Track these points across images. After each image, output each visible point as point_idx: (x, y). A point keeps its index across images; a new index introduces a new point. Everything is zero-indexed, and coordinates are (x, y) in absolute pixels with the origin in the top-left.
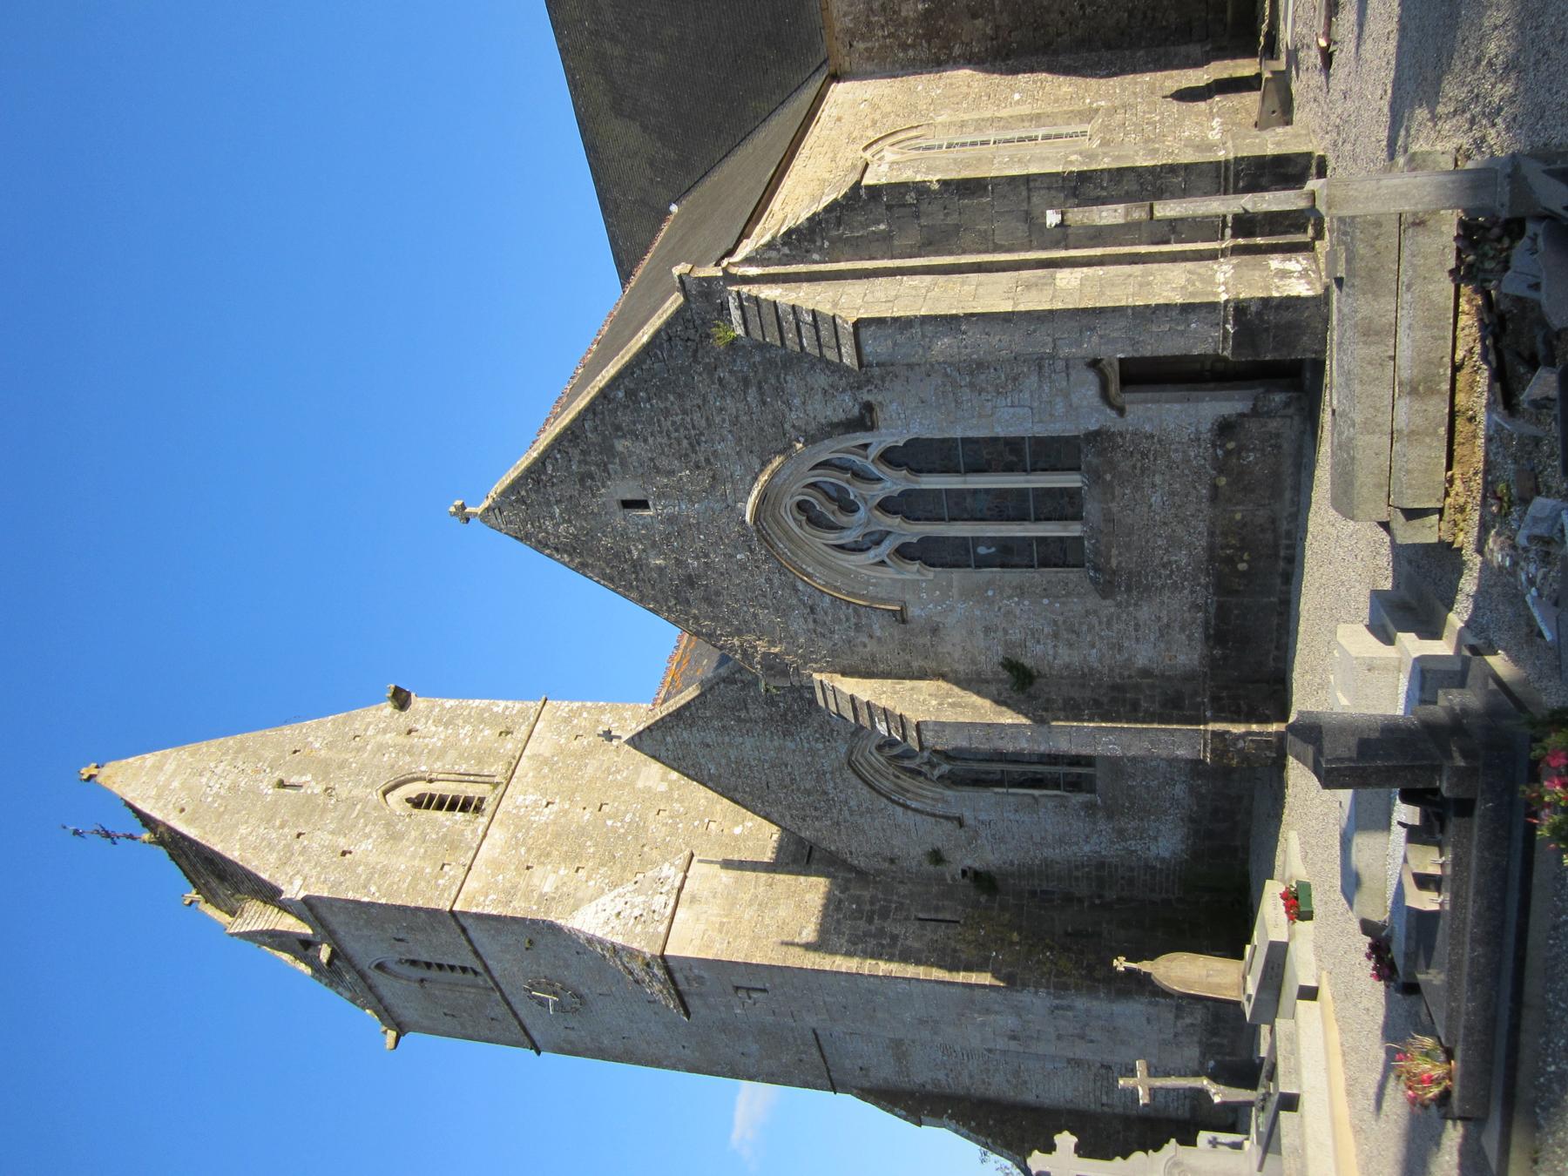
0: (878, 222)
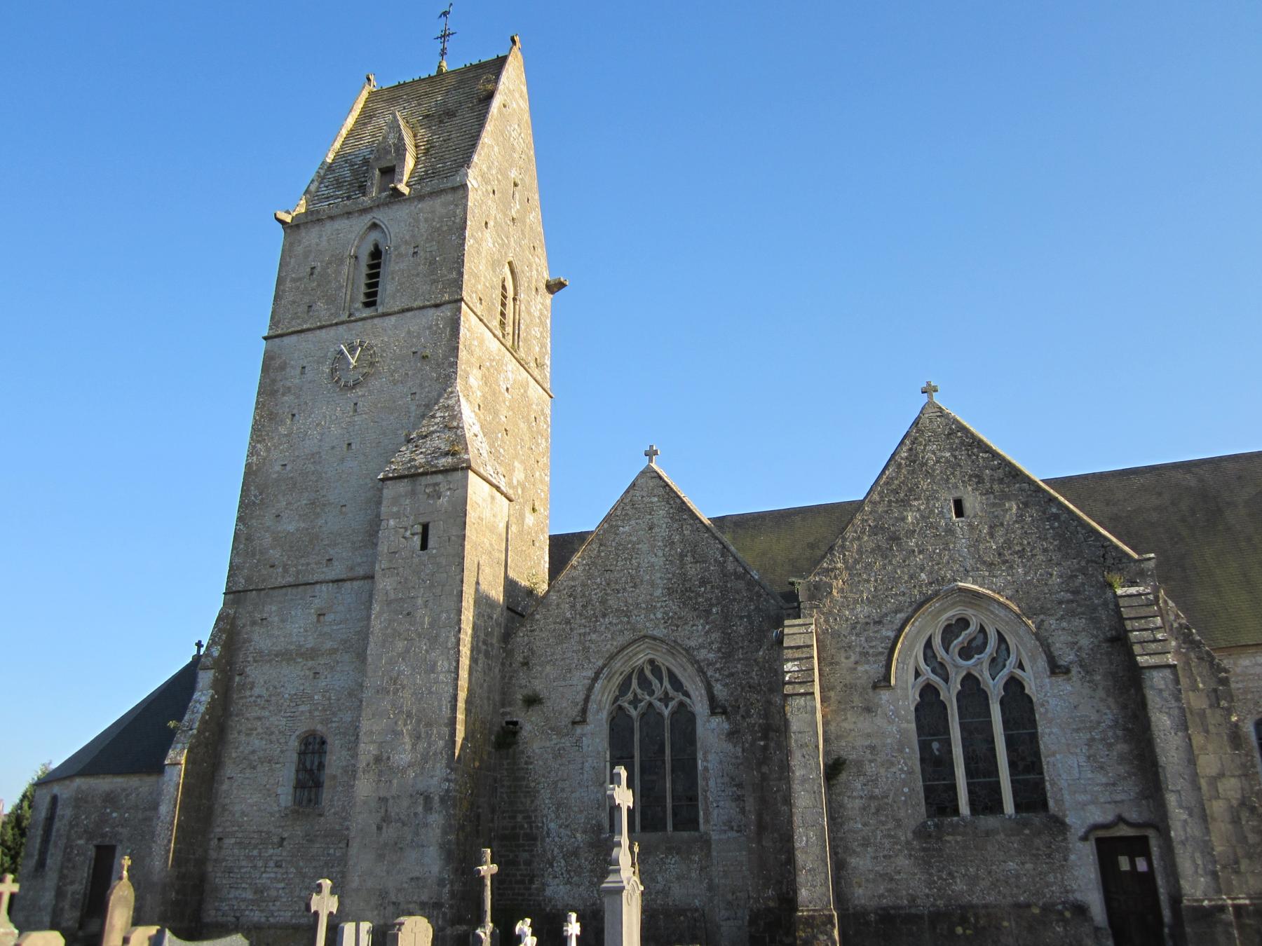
0: (1204, 683)
